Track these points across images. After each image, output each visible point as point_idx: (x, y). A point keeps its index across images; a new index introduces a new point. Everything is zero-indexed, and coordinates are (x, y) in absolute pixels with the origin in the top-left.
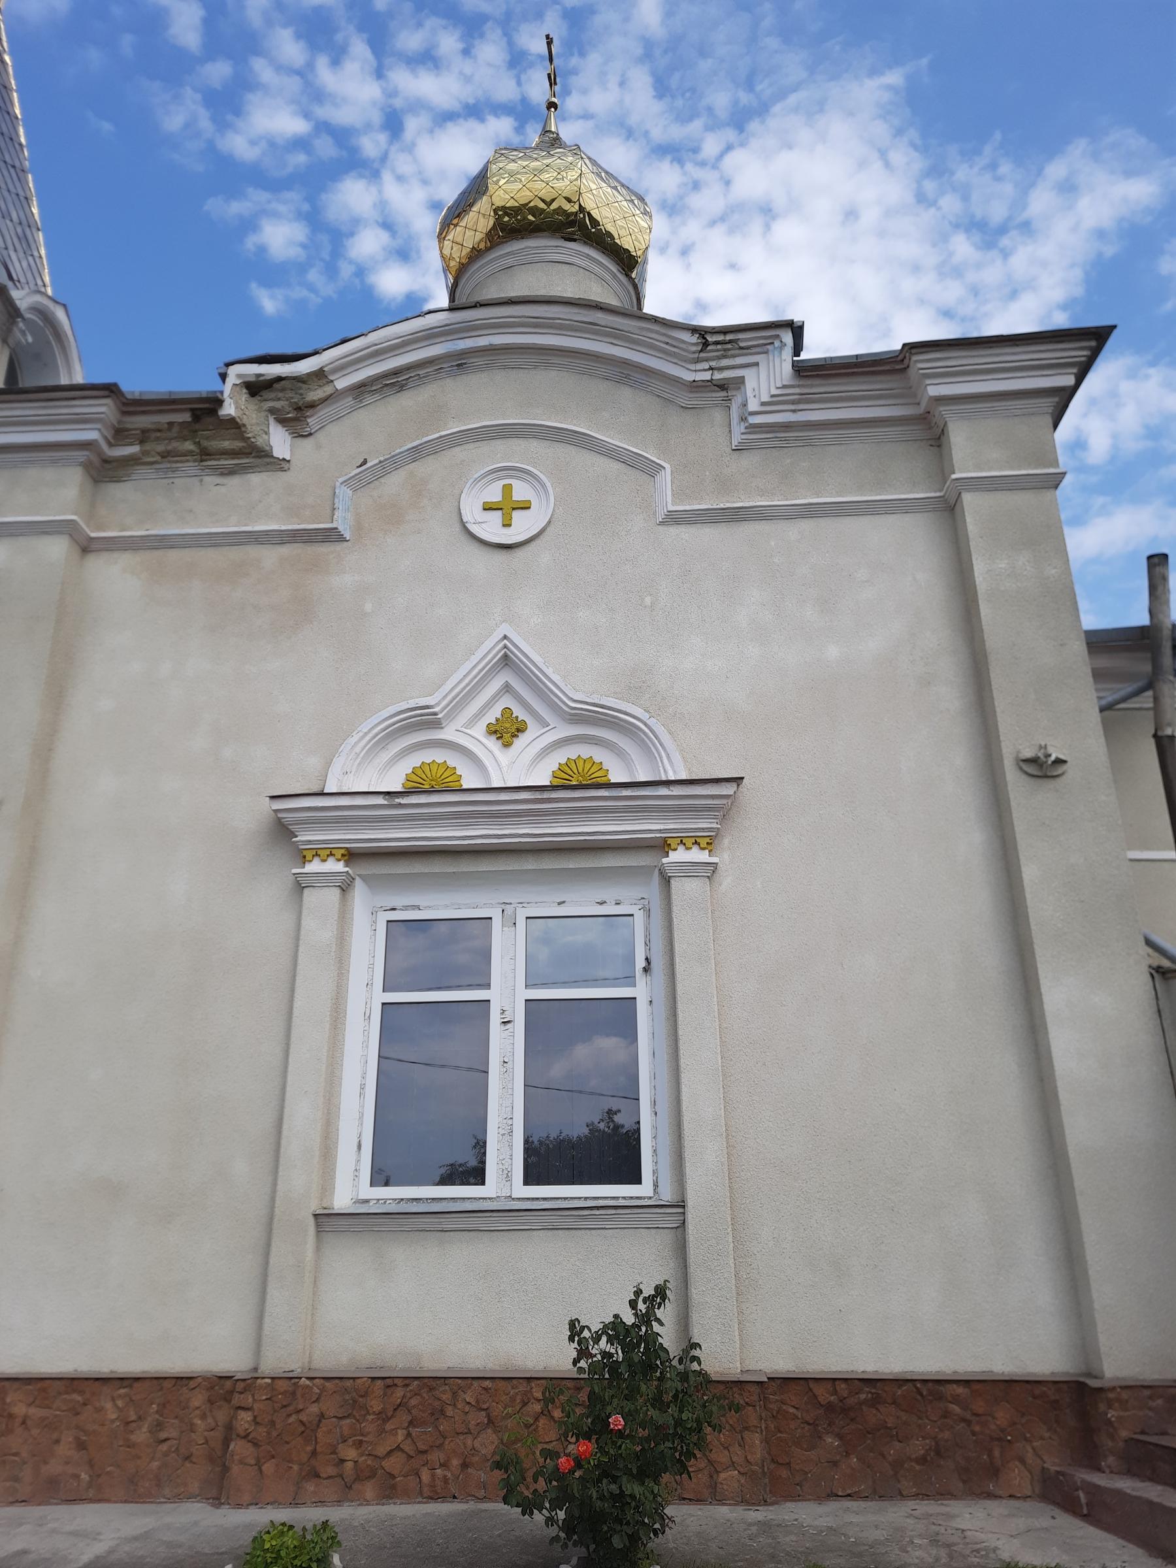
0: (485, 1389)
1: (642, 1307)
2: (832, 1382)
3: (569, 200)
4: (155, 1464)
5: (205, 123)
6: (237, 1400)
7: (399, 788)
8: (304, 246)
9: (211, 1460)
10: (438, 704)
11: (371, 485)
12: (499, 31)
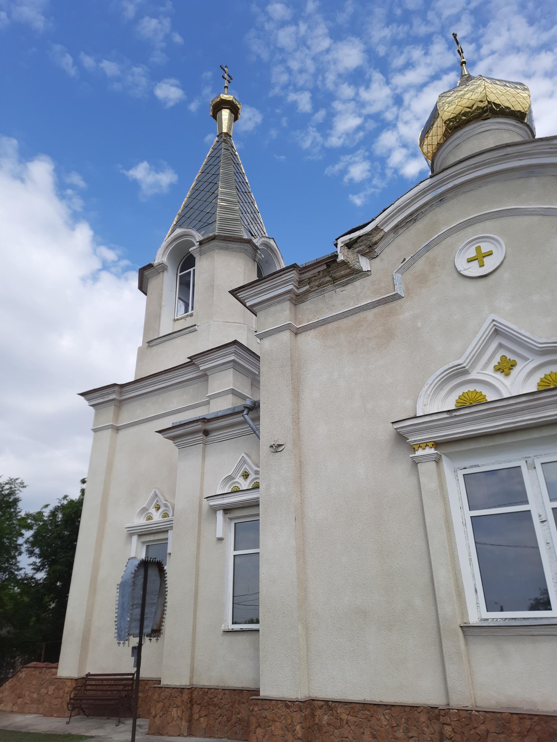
3: (482, 101)
5: (320, 139)
8: (369, 171)
10: (464, 362)
11: (410, 269)
12: (440, 36)
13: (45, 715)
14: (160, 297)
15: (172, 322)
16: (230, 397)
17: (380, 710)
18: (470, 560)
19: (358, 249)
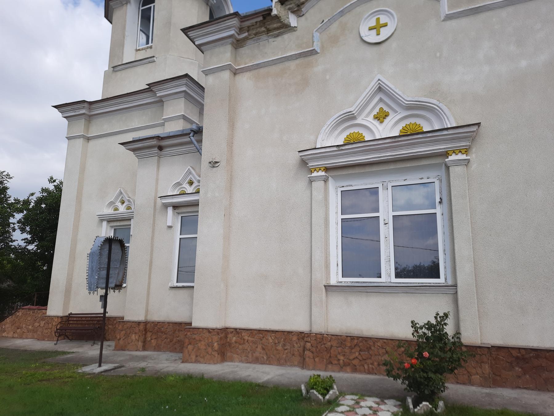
0: (385, 342)
1: (439, 319)
2: (519, 349)
4: (284, 356)
6: (305, 339)
7: (342, 143)
9: (300, 356)
13: (38, 340)
14: (124, 28)
15: (134, 52)
16: (181, 121)
17: (269, 334)
18: (337, 246)
19: (288, 7)
